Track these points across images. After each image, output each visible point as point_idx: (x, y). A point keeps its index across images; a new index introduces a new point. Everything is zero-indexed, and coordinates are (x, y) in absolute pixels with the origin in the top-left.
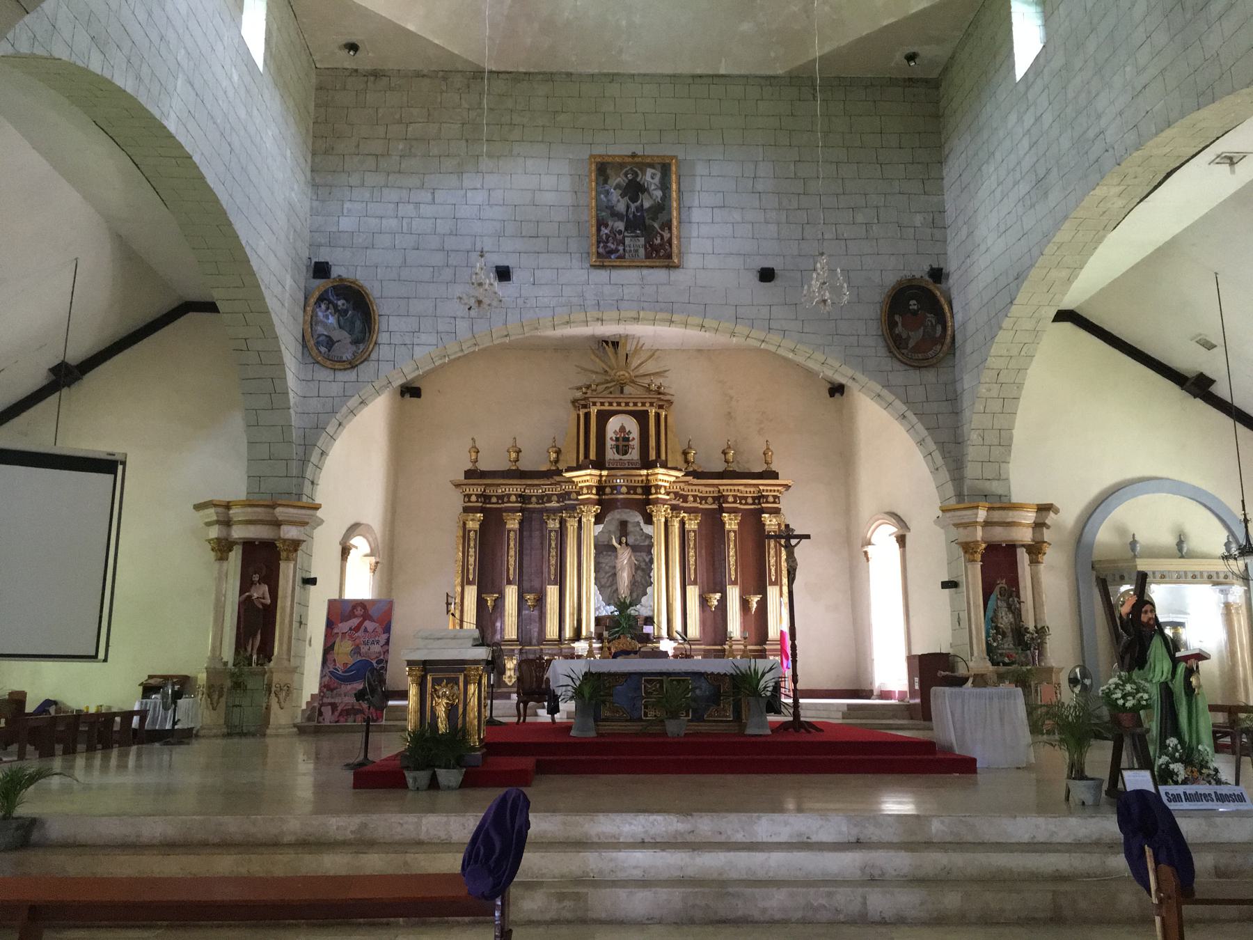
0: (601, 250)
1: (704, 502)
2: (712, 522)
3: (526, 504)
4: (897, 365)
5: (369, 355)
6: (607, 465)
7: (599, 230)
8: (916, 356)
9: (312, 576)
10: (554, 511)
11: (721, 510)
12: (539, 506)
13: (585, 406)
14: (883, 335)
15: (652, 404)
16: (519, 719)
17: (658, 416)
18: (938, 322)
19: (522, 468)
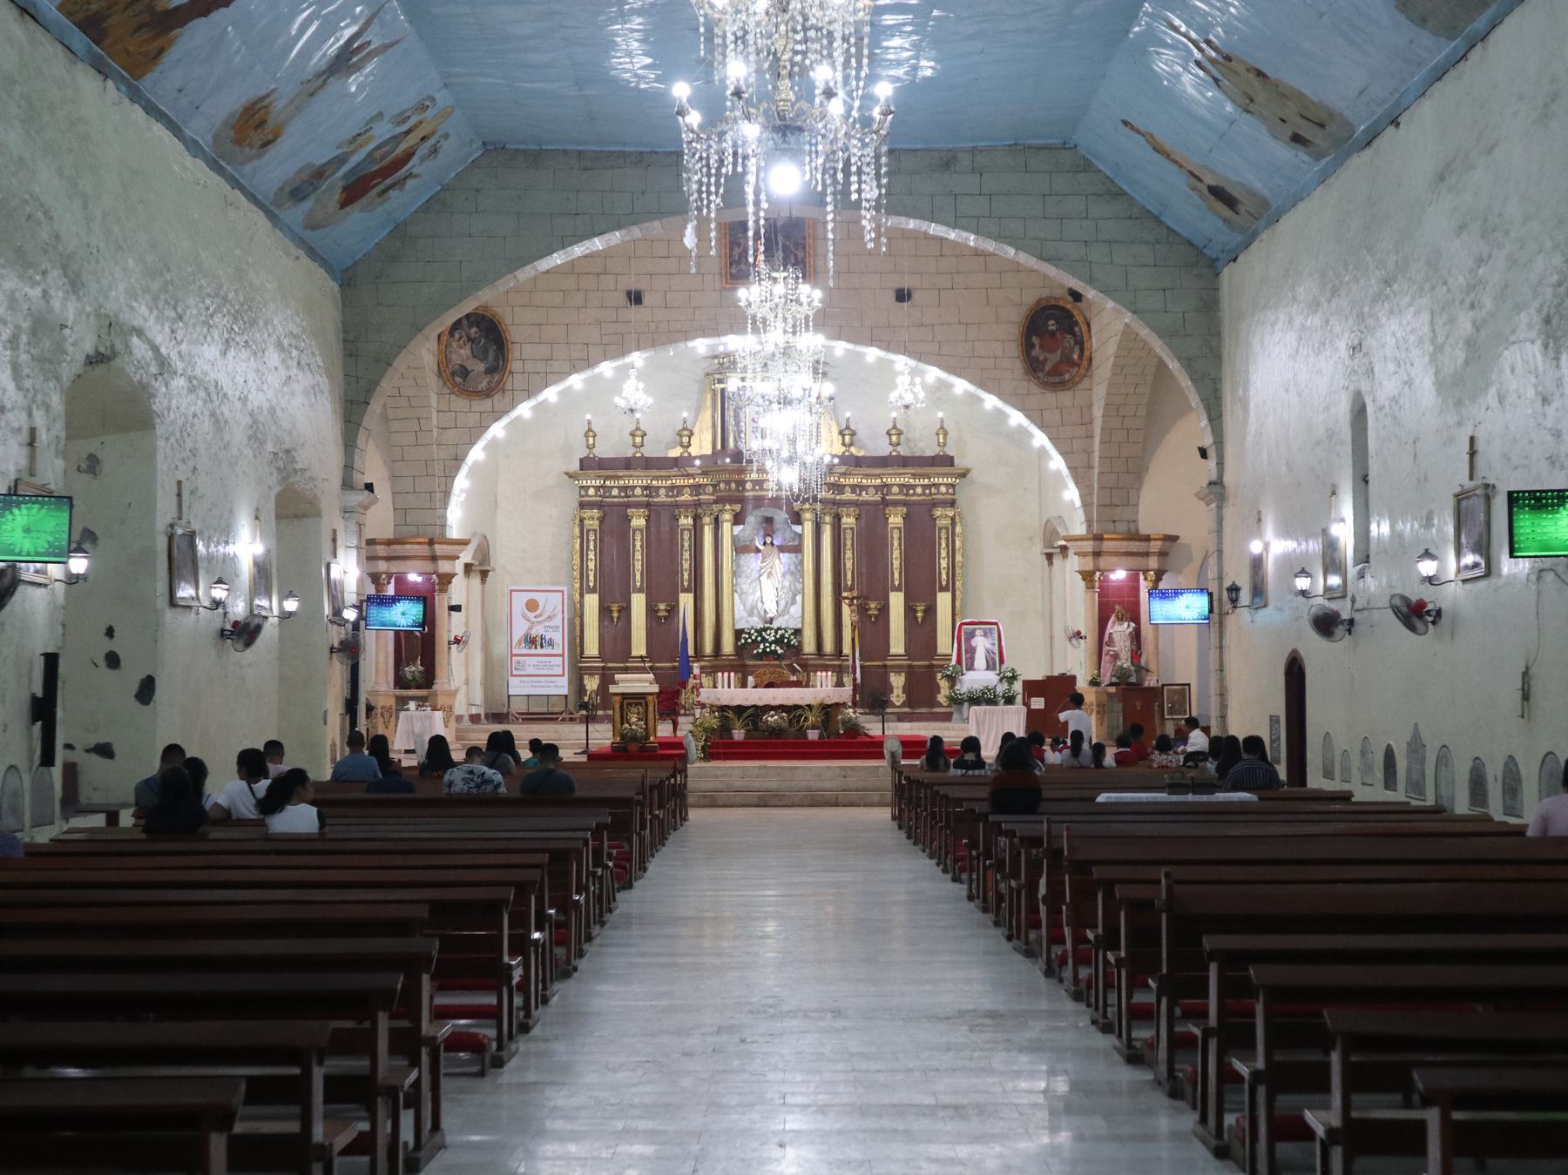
0: (734, 271)
2: (873, 516)
3: (653, 497)
4: (1034, 388)
7: (731, 249)
8: (1052, 380)
10: (686, 505)
12: (669, 500)
18: (1076, 342)
19: (646, 455)
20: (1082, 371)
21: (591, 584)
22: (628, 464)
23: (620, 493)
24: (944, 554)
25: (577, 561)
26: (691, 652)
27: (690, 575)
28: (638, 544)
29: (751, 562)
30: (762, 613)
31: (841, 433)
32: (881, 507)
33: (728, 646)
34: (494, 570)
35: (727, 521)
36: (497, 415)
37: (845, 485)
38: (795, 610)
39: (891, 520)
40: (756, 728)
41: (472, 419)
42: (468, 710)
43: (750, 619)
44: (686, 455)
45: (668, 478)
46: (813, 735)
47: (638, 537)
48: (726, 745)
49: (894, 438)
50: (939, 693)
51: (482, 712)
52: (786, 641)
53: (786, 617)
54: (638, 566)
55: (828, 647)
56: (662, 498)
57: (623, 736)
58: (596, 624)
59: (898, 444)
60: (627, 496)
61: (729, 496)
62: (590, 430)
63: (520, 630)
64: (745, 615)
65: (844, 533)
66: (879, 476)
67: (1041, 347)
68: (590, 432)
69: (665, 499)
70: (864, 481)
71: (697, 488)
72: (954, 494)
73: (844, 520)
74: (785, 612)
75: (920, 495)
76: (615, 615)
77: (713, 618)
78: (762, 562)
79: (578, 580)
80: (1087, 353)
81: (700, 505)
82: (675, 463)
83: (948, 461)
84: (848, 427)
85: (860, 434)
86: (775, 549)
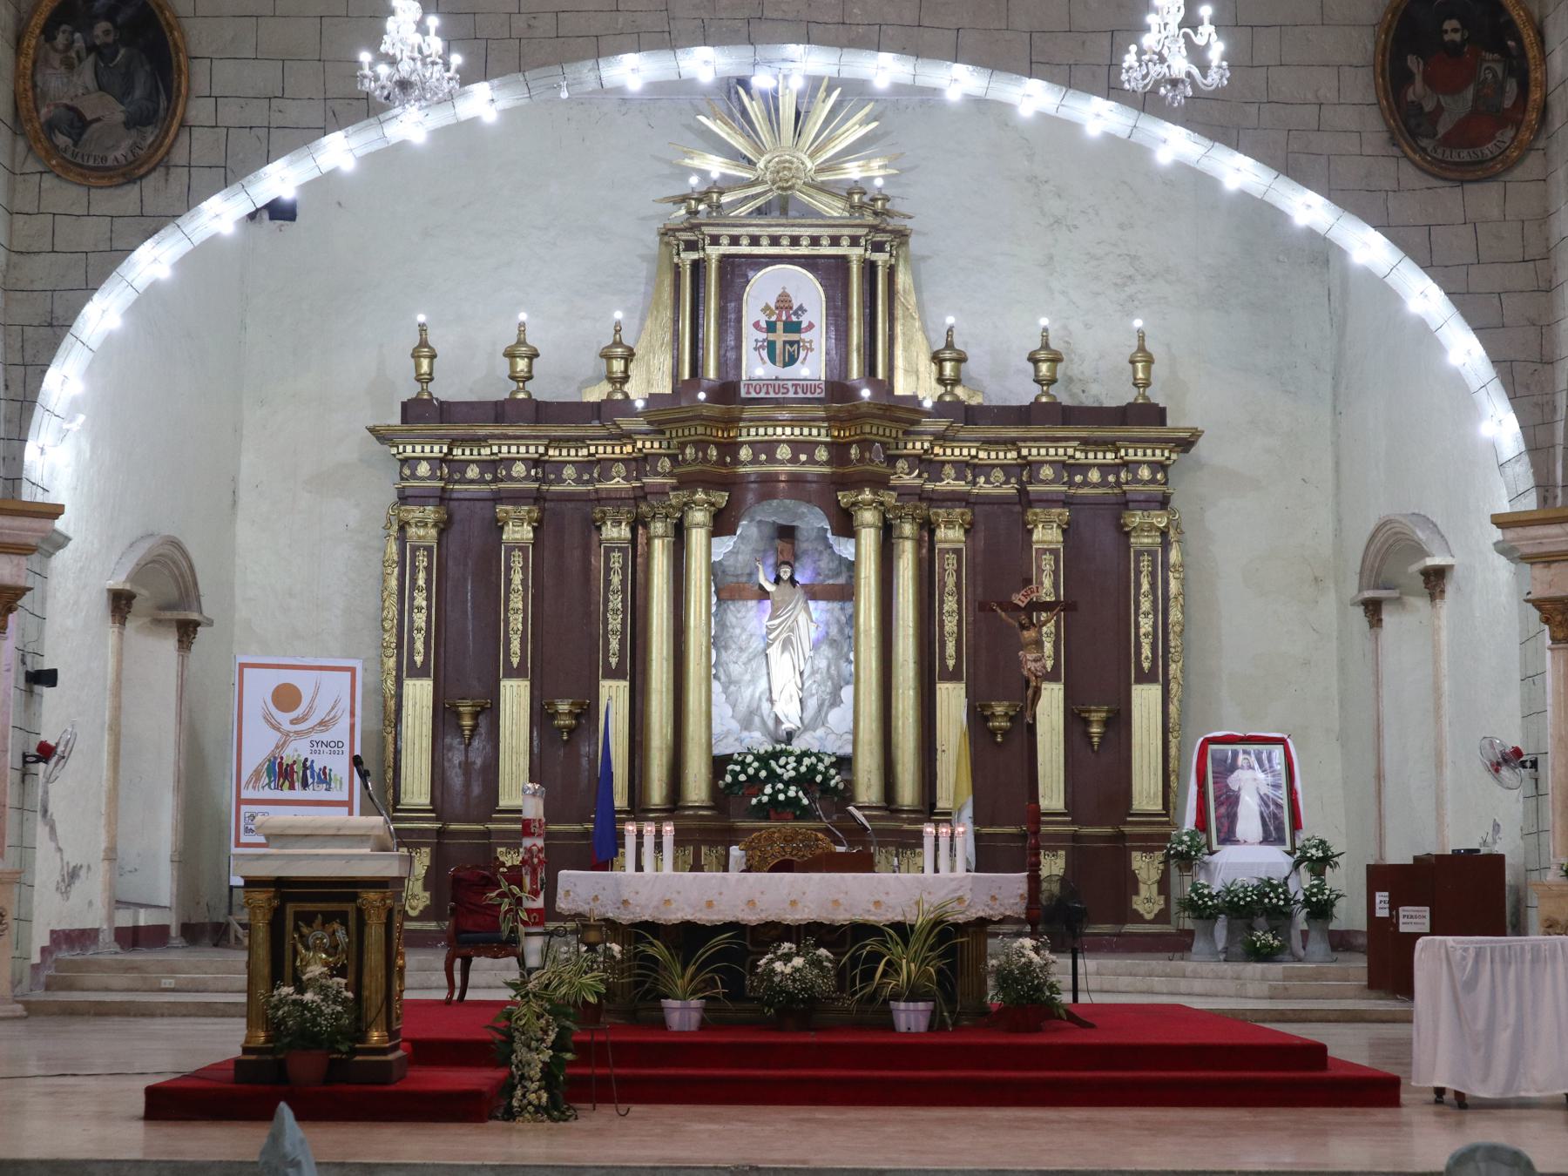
1: (982, 479)
3: (551, 483)
4: (1410, 175)
5: (168, 153)
6: (743, 394)
9: (47, 666)
11: (1024, 500)
13: (691, 246)
14: (1379, 103)
15: (854, 241)
16: (452, 993)
17: (870, 268)
18: (1510, 72)
19: (540, 396)
20: (1525, 135)
21: (419, 659)
22: (499, 412)
23: (482, 474)
24: (1146, 605)
25: (392, 612)
26: (620, 801)
27: (622, 643)
28: (517, 578)
29: (750, 619)
30: (771, 723)
31: (937, 359)
32: (1018, 508)
33: (697, 789)
34: (210, 623)
35: (698, 525)
36: (150, 224)
37: (943, 463)
38: (839, 718)
39: (1038, 535)
40: (736, 991)
41: (92, 232)
42: (110, 918)
43: (745, 734)
44: (619, 396)
45: (580, 441)
46: (910, 1017)
47: (517, 563)
48: (628, 1053)
49: (1044, 368)
50: (1137, 893)
51: (171, 920)
52: (819, 778)
53: (820, 732)
54: (516, 622)
55: (907, 794)
56: (569, 483)
57: (275, 1028)
58: (427, 742)
59: (1052, 381)
60: (495, 480)
61: (702, 472)
62: (424, 343)
63: (258, 746)
64: (735, 725)
65: (942, 559)
66: (1012, 443)
67: (1428, 80)
68: (423, 349)
69: (574, 488)
70: (982, 455)
71: (640, 463)
72: (1166, 483)
73: (941, 533)
74: (819, 719)
75: (1095, 486)
76: (467, 722)
77: (668, 731)
78: (770, 619)
79: (392, 651)
80: (1535, 95)
81: (644, 498)
82: (596, 411)
83: (1156, 415)
84: (949, 345)
85: (970, 368)
86: (799, 592)
